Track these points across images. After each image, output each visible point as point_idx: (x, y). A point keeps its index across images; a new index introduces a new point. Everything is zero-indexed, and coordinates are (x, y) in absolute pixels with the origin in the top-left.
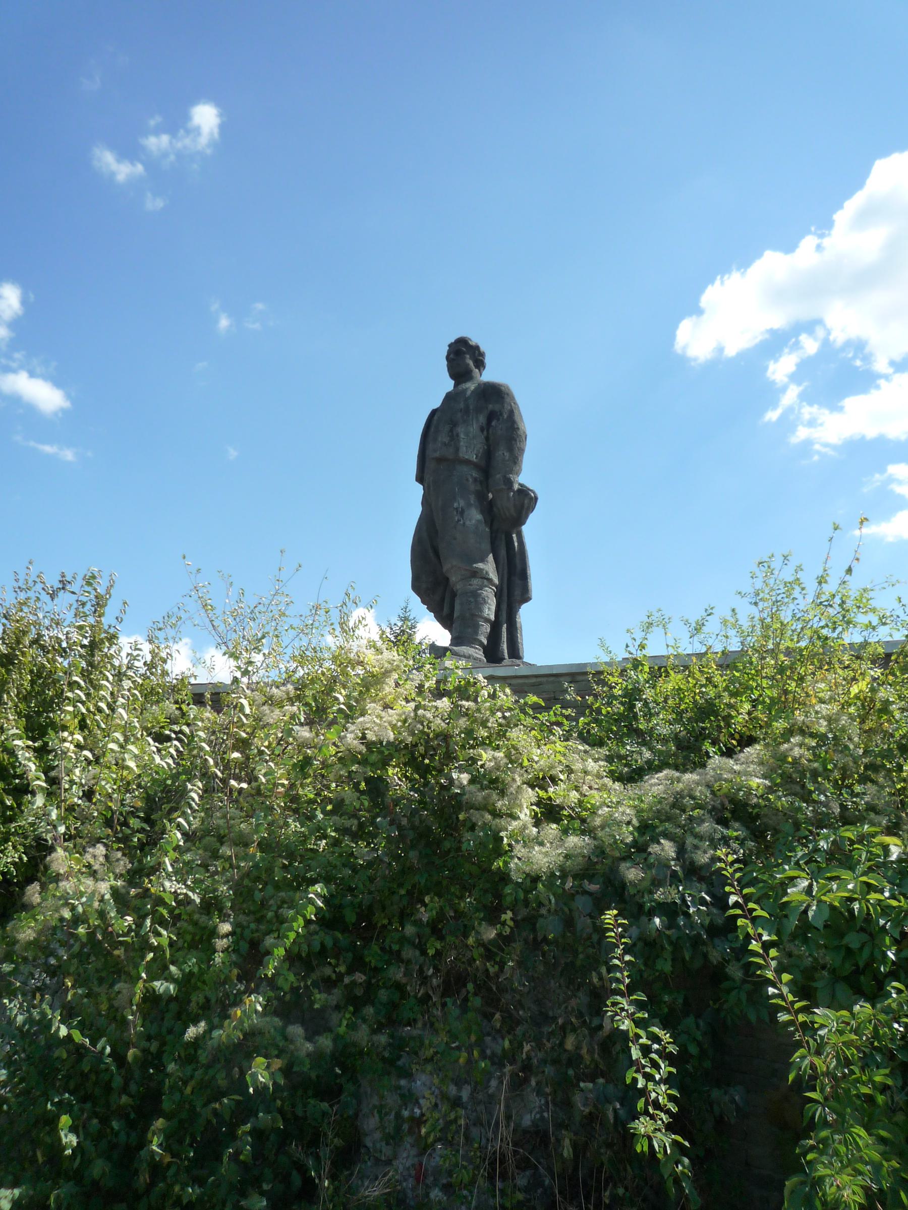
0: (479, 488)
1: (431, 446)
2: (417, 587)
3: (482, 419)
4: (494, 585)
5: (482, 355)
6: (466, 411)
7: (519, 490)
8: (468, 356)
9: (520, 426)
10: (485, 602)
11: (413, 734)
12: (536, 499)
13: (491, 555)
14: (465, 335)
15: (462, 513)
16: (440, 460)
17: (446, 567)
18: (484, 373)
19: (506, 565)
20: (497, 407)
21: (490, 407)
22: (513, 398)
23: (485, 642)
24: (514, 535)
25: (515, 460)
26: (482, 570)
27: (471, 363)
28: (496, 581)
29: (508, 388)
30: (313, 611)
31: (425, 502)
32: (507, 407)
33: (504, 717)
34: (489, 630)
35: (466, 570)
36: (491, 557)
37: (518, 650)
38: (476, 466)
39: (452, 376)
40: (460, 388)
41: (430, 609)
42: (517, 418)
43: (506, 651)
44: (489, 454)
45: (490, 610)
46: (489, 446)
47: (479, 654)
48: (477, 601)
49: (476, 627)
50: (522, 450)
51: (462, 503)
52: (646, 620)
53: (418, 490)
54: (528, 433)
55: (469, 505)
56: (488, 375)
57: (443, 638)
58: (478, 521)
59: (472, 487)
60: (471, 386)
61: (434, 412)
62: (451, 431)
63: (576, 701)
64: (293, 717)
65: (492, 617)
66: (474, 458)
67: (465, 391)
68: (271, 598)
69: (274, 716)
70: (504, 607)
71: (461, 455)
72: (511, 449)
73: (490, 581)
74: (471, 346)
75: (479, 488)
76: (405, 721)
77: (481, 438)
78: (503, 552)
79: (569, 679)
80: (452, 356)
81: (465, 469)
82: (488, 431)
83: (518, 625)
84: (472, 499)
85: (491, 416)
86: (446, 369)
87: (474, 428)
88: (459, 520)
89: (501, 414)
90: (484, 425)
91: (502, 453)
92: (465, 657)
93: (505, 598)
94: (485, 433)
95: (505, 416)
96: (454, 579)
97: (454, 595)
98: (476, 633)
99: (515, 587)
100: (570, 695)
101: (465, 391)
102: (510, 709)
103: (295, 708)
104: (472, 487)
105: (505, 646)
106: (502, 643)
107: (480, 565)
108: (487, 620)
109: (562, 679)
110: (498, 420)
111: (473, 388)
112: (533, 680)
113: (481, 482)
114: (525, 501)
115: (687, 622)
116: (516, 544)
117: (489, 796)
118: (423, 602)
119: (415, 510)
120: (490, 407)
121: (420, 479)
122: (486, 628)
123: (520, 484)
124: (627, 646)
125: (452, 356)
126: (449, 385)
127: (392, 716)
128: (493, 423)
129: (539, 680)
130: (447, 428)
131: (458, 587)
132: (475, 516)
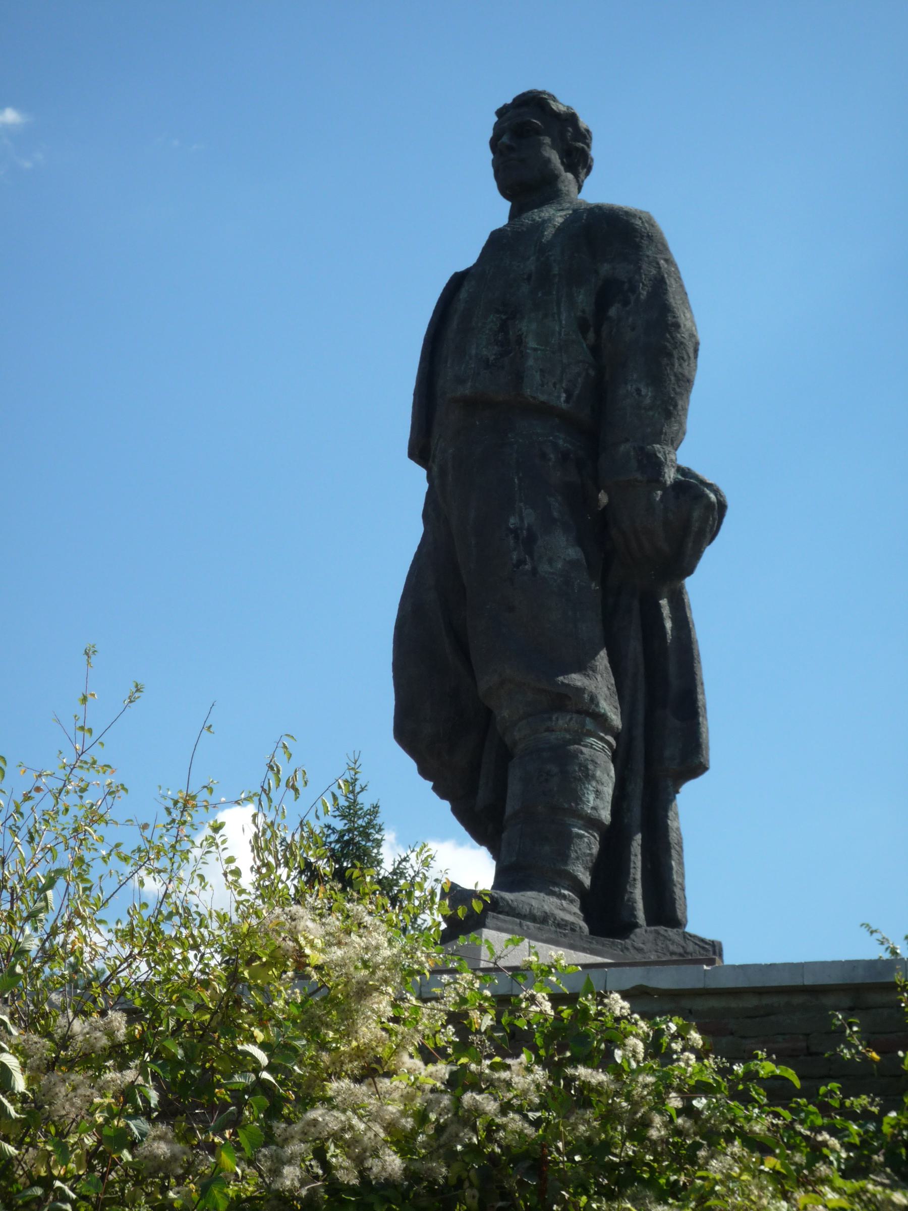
2: (408, 732)
3: (584, 299)
5: (584, 136)
7: (677, 484)
8: (547, 140)
9: (682, 320)
10: (588, 777)
11: (451, 1157)
12: (722, 507)
13: (603, 653)
14: (550, 90)
15: (529, 542)
16: (471, 404)
18: (589, 182)
21: (605, 269)
22: (663, 248)
23: (586, 879)
24: (664, 602)
26: (580, 691)
27: (555, 158)
28: (616, 720)
30: (176, 814)
31: (433, 511)
33: (688, 1111)
34: (595, 849)
36: (602, 659)
37: (673, 901)
39: (506, 190)
41: (442, 790)
42: (674, 300)
43: (640, 905)
44: (600, 391)
45: (599, 799)
47: (569, 911)
48: (571, 775)
49: (565, 841)
50: (686, 382)
53: (415, 481)
54: (701, 336)
56: (598, 190)
57: (472, 866)
60: (555, 216)
61: (458, 281)
62: (504, 327)
63: (866, 1060)
64: (127, 1093)
65: (605, 815)
67: (540, 226)
68: (62, 774)
69: (70, 1095)
70: (637, 788)
71: (528, 392)
73: (601, 720)
74: (557, 116)
76: (422, 1118)
78: (634, 647)
79: (846, 1002)
82: (598, 333)
83: (673, 836)
85: (608, 292)
86: (490, 171)
88: (521, 562)
89: (633, 289)
91: (634, 389)
92: (533, 918)
93: (639, 765)
94: (591, 335)
95: (644, 294)
96: (506, 713)
97: (505, 755)
98: (565, 857)
99: (666, 736)
100: (849, 1046)
101: (540, 226)
102: (703, 1089)
103: (130, 1075)
105: (638, 893)
106: (627, 886)
107: (576, 679)
108: (592, 823)
109: (828, 1001)
110: (626, 303)
111: (559, 220)
112: (752, 1002)
114: (695, 514)
116: (668, 625)
118: (425, 772)
119: (406, 533)
120: (605, 269)
121: (420, 451)
122: (589, 844)
125: (505, 139)
126: (497, 212)
127: (392, 1097)
128: (613, 312)
129: (766, 1000)
132: (563, 551)
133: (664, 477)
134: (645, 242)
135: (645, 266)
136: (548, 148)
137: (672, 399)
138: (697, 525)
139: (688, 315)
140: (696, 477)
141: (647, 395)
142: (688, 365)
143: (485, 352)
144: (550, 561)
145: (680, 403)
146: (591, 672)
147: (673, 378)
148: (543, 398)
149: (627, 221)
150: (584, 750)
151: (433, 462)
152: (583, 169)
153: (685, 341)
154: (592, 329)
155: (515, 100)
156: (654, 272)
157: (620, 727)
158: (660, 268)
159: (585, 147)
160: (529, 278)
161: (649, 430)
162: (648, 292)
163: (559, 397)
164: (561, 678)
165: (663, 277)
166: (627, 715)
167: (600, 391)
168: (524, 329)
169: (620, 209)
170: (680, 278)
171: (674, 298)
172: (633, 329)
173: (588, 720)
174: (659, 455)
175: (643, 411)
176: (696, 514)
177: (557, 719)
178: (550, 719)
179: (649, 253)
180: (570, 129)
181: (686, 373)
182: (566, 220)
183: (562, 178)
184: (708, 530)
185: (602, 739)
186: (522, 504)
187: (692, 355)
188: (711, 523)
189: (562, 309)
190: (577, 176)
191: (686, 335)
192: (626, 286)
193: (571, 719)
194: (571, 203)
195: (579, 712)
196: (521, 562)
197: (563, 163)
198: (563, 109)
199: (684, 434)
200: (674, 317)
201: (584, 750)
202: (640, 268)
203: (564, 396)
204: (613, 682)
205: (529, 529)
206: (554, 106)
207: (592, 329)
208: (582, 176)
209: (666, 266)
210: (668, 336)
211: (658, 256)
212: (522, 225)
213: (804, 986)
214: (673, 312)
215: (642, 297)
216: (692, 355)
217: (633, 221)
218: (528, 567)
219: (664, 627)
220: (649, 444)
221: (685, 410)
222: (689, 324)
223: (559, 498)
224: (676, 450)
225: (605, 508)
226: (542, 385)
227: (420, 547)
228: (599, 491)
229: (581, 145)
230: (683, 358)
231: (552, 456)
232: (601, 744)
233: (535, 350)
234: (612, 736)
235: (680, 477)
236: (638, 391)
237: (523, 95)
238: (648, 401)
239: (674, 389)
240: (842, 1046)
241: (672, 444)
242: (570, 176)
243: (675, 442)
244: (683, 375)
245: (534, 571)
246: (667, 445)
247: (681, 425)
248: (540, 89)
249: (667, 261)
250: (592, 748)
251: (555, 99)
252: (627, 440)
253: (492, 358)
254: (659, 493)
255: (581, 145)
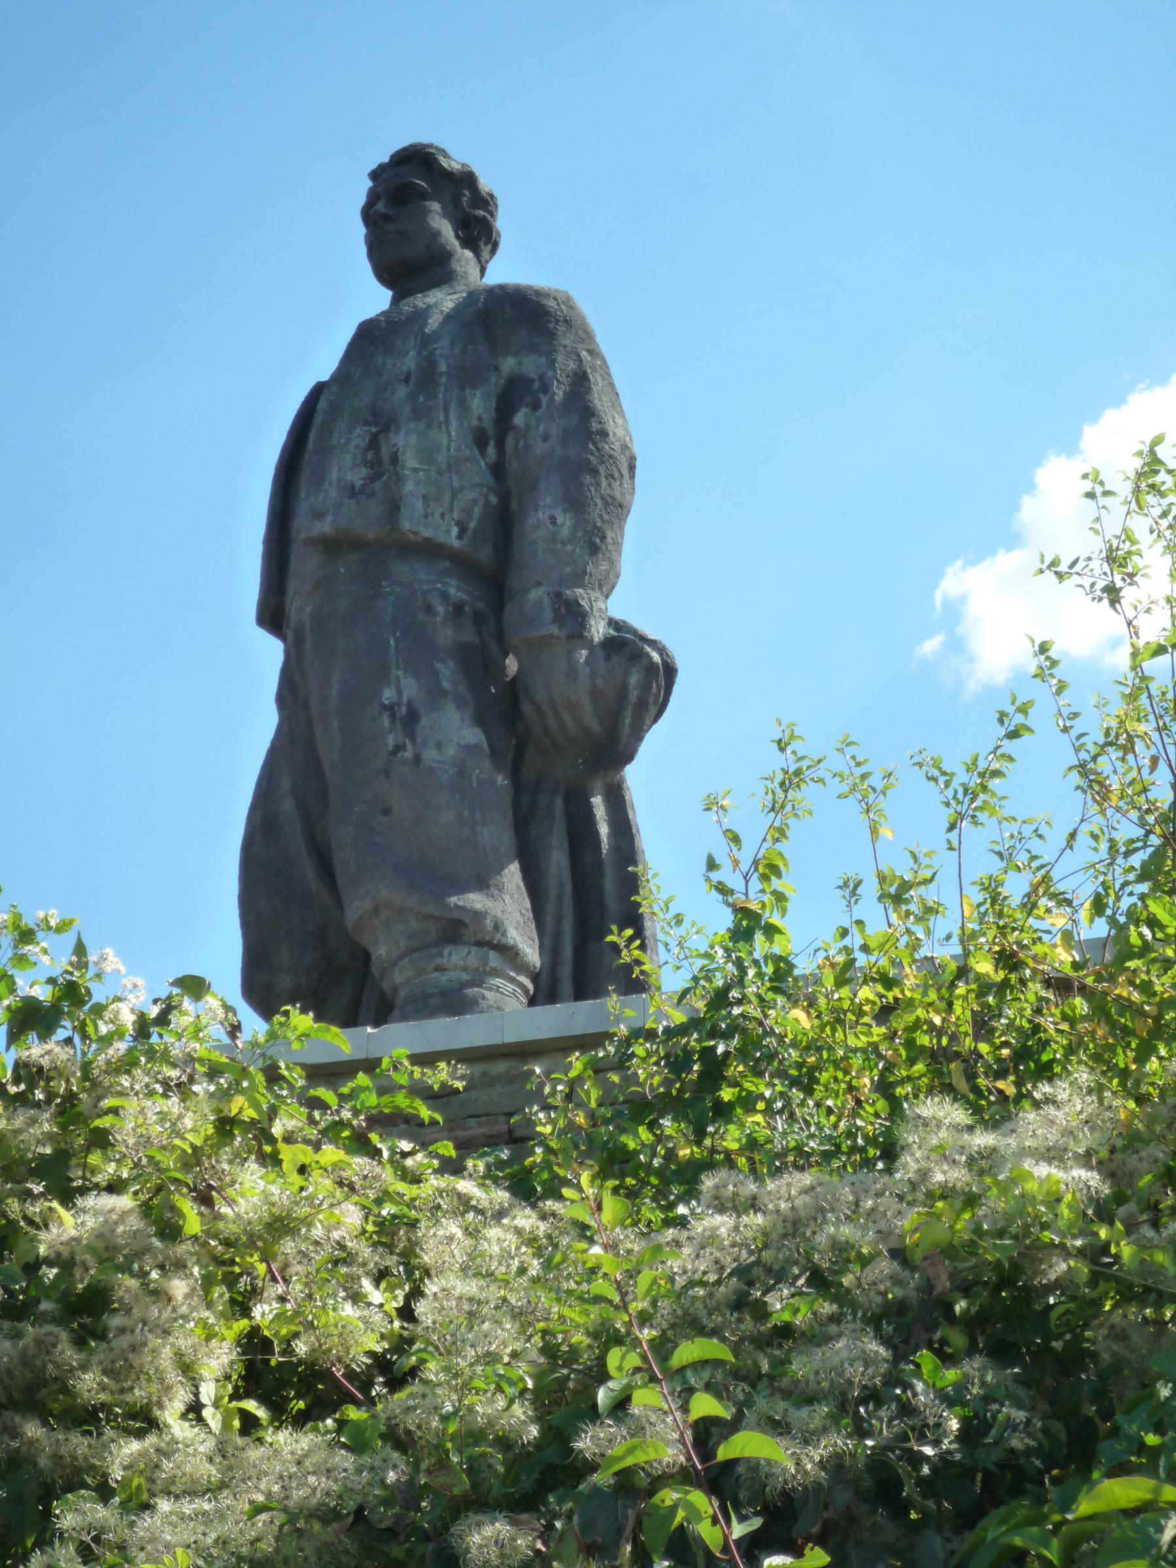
0: (469, 635)
1: (304, 504)
3: (480, 405)
4: (523, 968)
5: (486, 202)
6: (426, 378)
9: (610, 427)
12: (670, 671)
14: (425, 140)
15: (411, 720)
16: (332, 546)
17: (355, 909)
18: (492, 267)
19: (568, 902)
20: (530, 365)
21: (508, 364)
22: (587, 336)
24: (597, 801)
25: (595, 541)
26: (479, 916)
27: (446, 231)
28: (532, 954)
29: (569, 302)
32: (565, 364)
35: (428, 917)
36: (512, 874)
38: (461, 563)
40: (407, 306)
42: (599, 400)
46: (505, 497)
50: (618, 509)
51: (410, 688)
52: (778, 762)
55: (436, 695)
58: (471, 750)
59: (446, 635)
60: (443, 301)
61: (318, 390)
62: (374, 444)
66: (451, 537)
67: (421, 315)
71: (406, 525)
72: (577, 504)
73: (510, 953)
74: (448, 175)
75: (469, 635)
77: (479, 468)
78: (558, 861)
80: (380, 206)
81: (419, 575)
84: (447, 673)
87: (452, 436)
88: (399, 748)
89: (545, 388)
90: (489, 427)
91: (547, 519)
94: (491, 450)
95: (559, 394)
101: (421, 315)
104: (446, 635)
107: (475, 900)
110: (536, 406)
113: (478, 619)
114: (638, 679)
115: (938, 774)
116: (604, 830)
117: (45, 1346)
120: (508, 364)
121: (272, 616)
123: (612, 623)
124: (712, 865)
128: (519, 419)
130: (360, 436)
131: (398, 978)
132: (455, 732)
133: (590, 631)
134: (561, 329)
135: (560, 358)
136: (437, 217)
137: (599, 529)
138: (635, 694)
139: (620, 421)
140: (634, 631)
141: (564, 524)
142: (621, 485)
143: (349, 477)
144: (439, 746)
145: (610, 535)
146: (495, 892)
147: (599, 502)
148: (427, 533)
149: (538, 303)
150: (487, 994)
151: (288, 627)
152: (486, 244)
153: (615, 454)
154: (492, 443)
155: (392, 157)
156: (572, 365)
157: (538, 964)
158: (581, 361)
159: (487, 215)
160: (407, 380)
161: (568, 570)
162: (565, 392)
163: (448, 532)
164: (454, 900)
165: (585, 374)
166: (550, 950)
167: (503, 524)
168: (400, 445)
169: (530, 287)
170: (609, 375)
171: (600, 399)
172: (545, 440)
173: (492, 954)
174: (582, 603)
175: (559, 545)
176: (634, 679)
177: (450, 954)
178: (441, 954)
179: (567, 342)
180: (467, 193)
181: (617, 495)
182: (457, 305)
183: (457, 256)
184: (651, 700)
185: (512, 980)
186: (400, 672)
187: (625, 472)
188: (654, 691)
189: (451, 417)
190: (477, 253)
191: (617, 447)
192: (536, 385)
193: (468, 954)
194: (467, 285)
195: (480, 944)
196: (399, 748)
197: (457, 236)
198: (456, 166)
199: (618, 576)
200: (600, 423)
201: (487, 994)
202: (554, 361)
203: (455, 530)
204: (529, 905)
205: (410, 704)
206: (444, 163)
207: (492, 443)
208: (485, 254)
209: (589, 358)
210: (591, 446)
211: (579, 346)
212: (400, 313)
213: (505, 1045)
214: (599, 416)
215: (556, 398)
216: (625, 472)
217: (545, 302)
218: (408, 754)
219: (597, 833)
220: (568, 588)
221: (618, 545)
222: (620, 432)
223: (451, 664)
224: (607, 597)
225: (514, 679)
226: (426, 517)
227: (275, 742)
228: (506, 655)
229: (481, 213)
230: (612, 476)
231: (441, 609)
232: (511, 987)
233: (416, 470)
234: (528, 977)
235: (612, 632)
236: (553, 519)
237: (404, 150)
238: (565, 532)
239: (601, 516)
240: (536, 1108)
241: (600, 588)
242: (468, 254)
243: (606, 586)
244: (614, 499)
245: (417, 759)
246: (593, 589)
247: (613, 564)
248: (425, 141)
249: (589, 351)
250: (498, 991)
251: (445, 154)
252: (539, 584)
253: (359, 484)
254: (584, 652)
255: (481, 213)
